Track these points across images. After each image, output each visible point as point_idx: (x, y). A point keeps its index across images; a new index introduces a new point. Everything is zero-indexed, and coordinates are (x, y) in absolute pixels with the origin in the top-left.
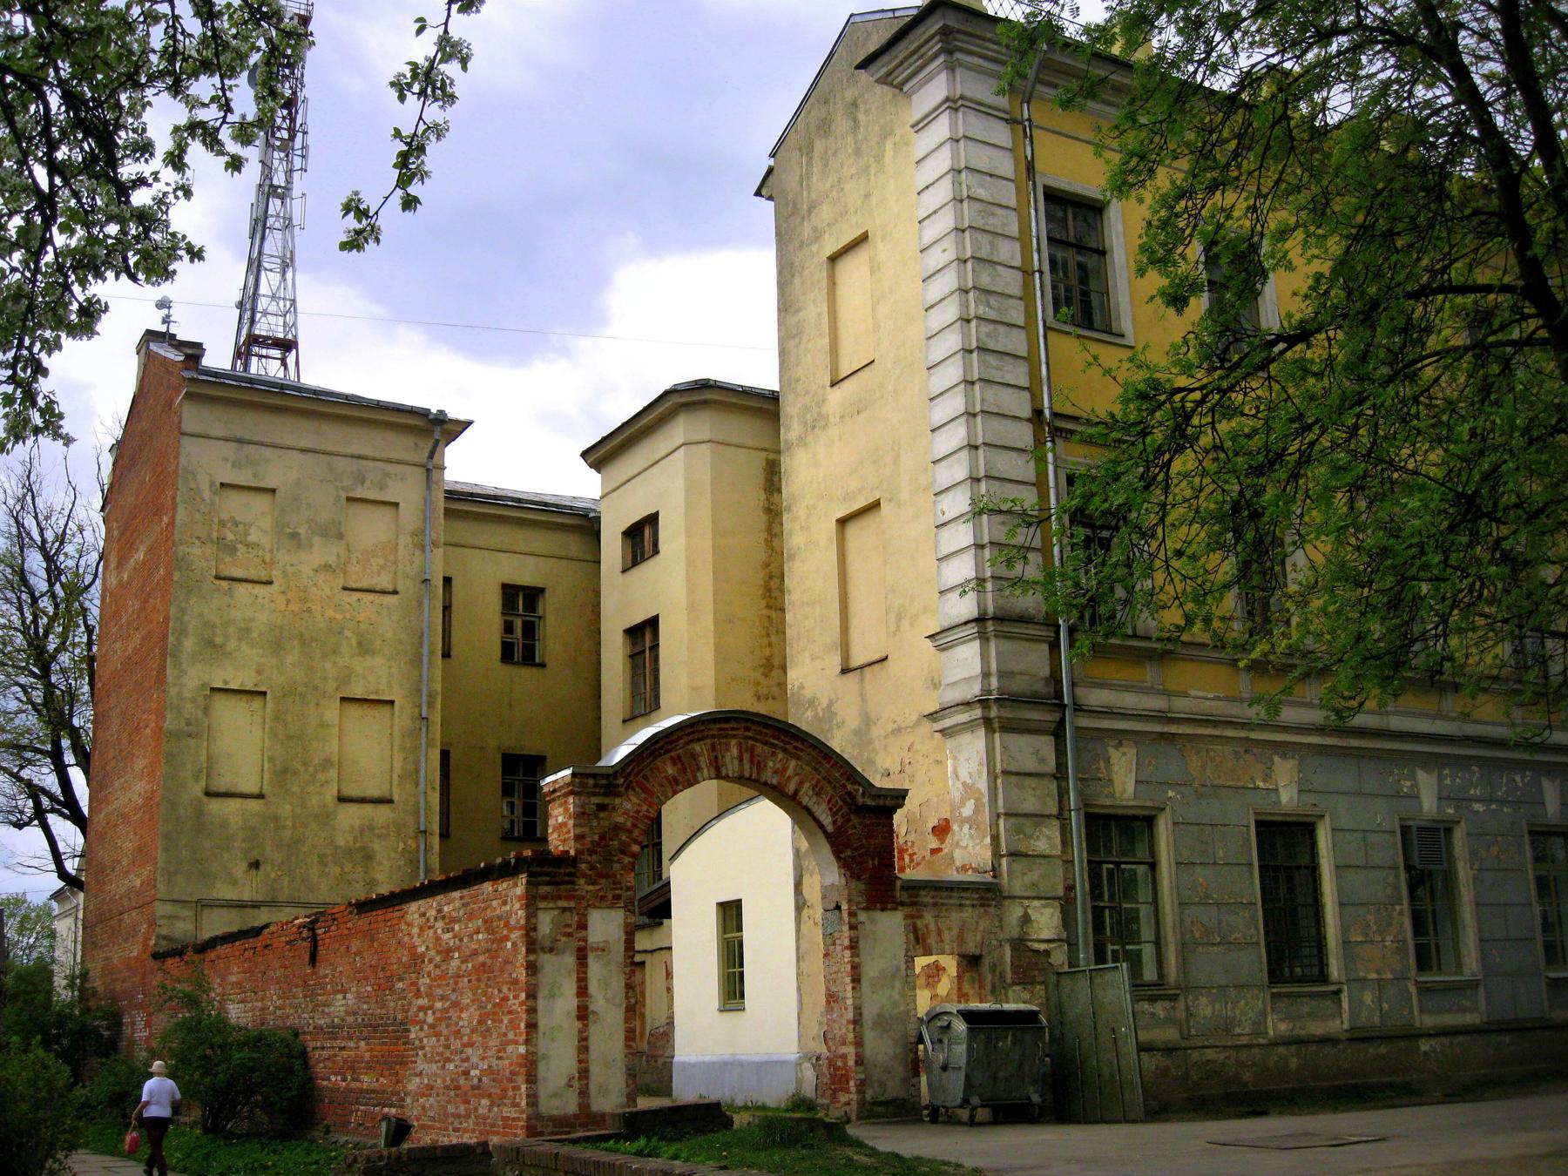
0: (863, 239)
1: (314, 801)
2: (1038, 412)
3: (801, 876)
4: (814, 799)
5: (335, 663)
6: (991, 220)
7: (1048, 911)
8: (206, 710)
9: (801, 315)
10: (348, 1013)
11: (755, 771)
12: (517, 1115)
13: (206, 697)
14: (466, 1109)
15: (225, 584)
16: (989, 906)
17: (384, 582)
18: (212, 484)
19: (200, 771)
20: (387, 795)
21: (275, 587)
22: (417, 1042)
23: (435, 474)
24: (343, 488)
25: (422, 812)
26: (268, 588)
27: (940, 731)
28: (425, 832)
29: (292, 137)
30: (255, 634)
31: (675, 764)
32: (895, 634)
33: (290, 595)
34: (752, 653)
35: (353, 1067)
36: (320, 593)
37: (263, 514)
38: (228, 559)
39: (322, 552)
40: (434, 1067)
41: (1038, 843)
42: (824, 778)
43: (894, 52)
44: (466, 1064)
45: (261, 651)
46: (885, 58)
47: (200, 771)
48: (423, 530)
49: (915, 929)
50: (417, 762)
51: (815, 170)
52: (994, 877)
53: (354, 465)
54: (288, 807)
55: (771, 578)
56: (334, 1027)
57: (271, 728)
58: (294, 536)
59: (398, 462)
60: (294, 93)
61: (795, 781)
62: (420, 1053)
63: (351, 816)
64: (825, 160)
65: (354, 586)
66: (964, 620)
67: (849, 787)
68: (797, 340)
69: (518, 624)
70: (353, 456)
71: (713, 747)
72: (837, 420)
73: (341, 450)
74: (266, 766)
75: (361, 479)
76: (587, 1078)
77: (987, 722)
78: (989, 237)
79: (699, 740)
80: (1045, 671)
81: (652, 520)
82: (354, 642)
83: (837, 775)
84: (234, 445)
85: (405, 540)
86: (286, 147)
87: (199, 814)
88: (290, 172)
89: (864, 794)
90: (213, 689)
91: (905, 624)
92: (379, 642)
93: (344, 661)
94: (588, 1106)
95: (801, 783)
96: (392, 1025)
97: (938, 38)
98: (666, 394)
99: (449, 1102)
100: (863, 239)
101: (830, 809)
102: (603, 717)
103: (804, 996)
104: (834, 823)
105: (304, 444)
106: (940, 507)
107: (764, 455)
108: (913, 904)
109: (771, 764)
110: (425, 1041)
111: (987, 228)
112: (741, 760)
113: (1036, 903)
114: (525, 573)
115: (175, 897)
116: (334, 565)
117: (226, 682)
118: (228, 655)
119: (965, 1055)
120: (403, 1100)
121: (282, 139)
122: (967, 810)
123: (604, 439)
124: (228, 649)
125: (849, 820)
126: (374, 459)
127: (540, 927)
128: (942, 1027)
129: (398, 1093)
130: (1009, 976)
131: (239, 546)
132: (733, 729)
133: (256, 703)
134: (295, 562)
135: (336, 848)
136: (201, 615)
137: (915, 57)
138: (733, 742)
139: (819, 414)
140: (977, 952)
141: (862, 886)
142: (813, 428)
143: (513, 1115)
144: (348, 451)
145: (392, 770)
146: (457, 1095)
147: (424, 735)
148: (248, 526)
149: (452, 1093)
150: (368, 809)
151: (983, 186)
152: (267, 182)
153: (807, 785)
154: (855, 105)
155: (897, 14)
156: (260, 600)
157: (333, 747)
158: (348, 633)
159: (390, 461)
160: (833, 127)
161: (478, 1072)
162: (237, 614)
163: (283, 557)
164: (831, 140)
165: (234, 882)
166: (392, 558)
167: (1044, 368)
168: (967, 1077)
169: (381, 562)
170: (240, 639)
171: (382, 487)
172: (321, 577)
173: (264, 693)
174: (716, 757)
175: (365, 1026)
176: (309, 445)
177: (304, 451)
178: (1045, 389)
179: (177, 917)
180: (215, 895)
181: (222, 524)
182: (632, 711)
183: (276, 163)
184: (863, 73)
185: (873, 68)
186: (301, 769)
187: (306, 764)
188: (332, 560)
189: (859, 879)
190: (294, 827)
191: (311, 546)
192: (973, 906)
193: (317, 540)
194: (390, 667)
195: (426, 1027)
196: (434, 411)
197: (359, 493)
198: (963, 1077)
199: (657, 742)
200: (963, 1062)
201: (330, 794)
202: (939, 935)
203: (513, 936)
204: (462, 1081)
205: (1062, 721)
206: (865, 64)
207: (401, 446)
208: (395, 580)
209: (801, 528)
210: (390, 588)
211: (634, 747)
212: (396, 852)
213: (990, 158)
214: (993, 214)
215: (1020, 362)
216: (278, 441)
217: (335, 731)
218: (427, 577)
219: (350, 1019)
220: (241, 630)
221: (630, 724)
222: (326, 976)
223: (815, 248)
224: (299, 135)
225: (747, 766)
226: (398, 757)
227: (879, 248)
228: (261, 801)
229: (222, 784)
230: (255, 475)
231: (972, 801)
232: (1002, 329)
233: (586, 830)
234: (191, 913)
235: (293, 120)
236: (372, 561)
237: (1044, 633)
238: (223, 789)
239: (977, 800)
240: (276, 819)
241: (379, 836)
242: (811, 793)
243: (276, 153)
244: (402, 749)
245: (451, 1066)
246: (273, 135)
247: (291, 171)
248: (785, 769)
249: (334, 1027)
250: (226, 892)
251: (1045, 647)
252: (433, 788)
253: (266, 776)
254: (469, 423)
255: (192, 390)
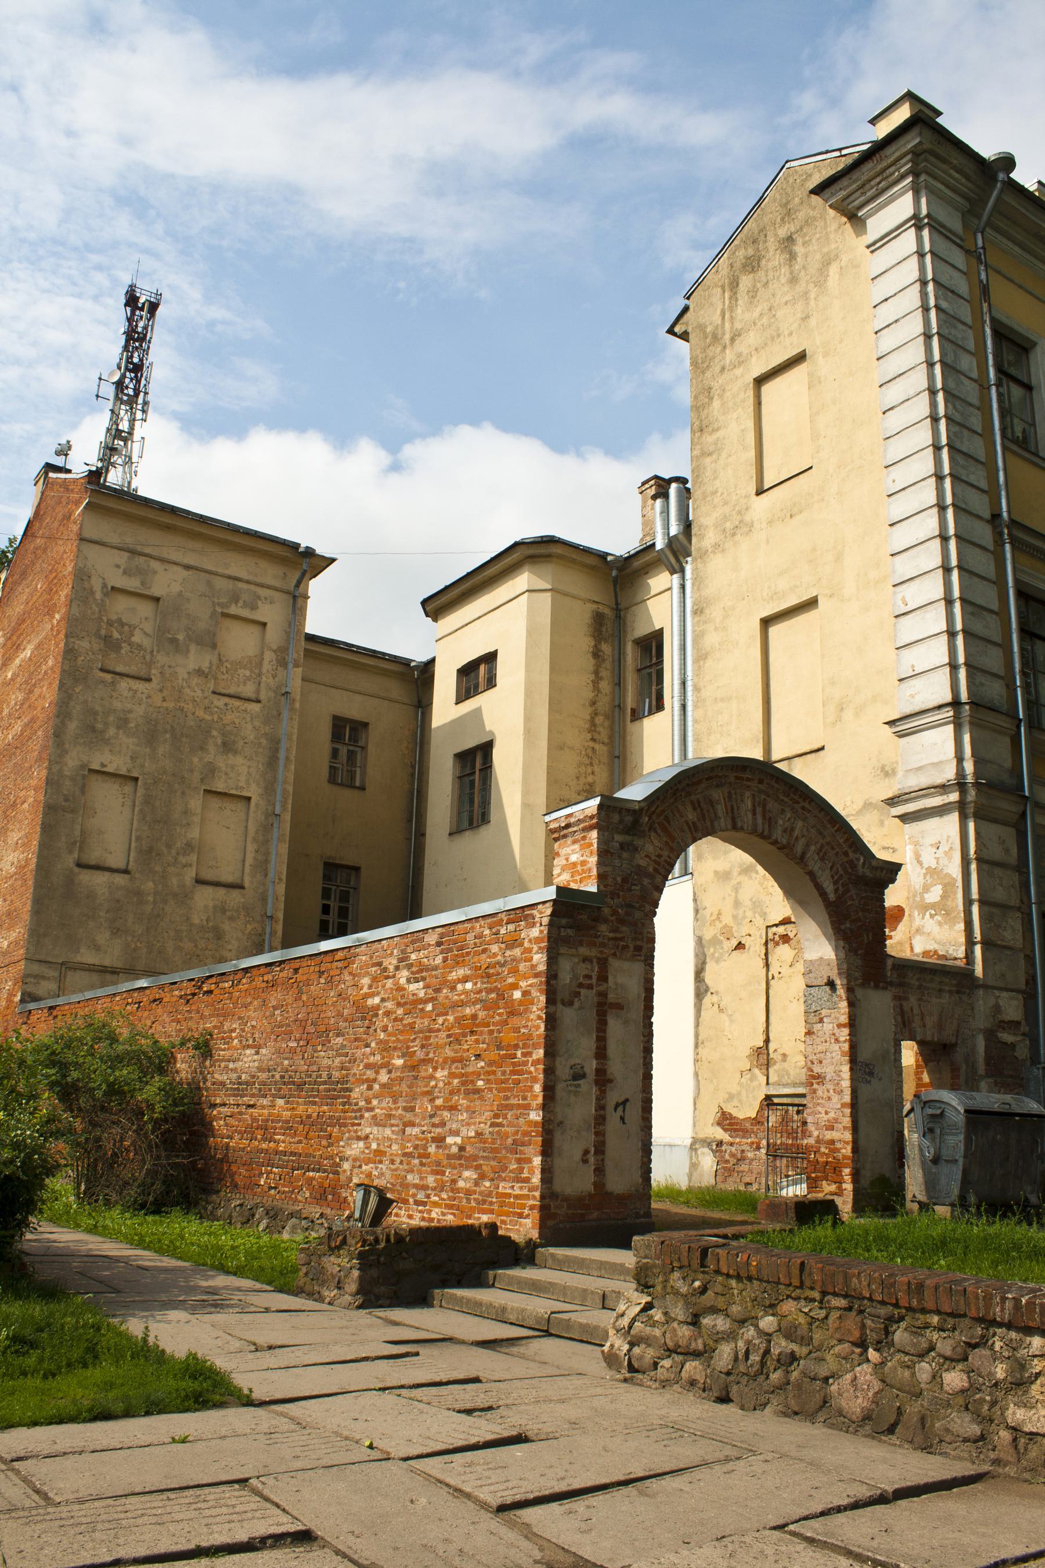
0: (800, 358)
1: (175, 881)
2: (996, 516)
3: (704, 963)
4: (819, 864)
5: (201, 759)
6: (953, 332)
7: (1015, 1003)
8: (83, 791)
9: (720, 434)
10: (260, 1069)
11: (766, 827)
12: (525, 1192)
13: (84, 777)
14: (436, 1180)
15: (108, 677)
16: (964, 993)
17: (248, 690)
18: (105, 586)
19: (74, 843)
20: (239, 881)
21: (154, 684)
22: (362, 1103)
23: (300, 601)
24: (219, 604)
25: (270, 900)
26: (147, 685)
27: (898, 817)
28: (271, 917)
29: (137, 395)
30: (132, 725)
31: (695, 809)
32: (834, 724)
33: (166, 693)
34: (578, 778)
35: (265, 1129)
36: (192, 694)
37: (146, 619)
38: (113, 655)
39: (197, 659)
40: (388, 1132)
41: (1005, 934)
42: (828, 843)
43: (855, 175)
44: (439, 1130)
45: (136, 740)
46: (845, 182)
47: (74, 843)
48: (287, 649)
49: (902, 1013)
50: (267, 854)
51: (740, 302)
52: (968, 964)
53: (228, 585)
54: (151, 884)
55: (596, 714)
56: (240, 1084)
57: (141, 811)
58: (174, 641)
59: (269, 587)
60: (141, 360)
61: (802, 842)
62: (367, 1115)
63: (205, 898)
64: (753, 293)
65: (223, 691)
66: (936, 703)
67: (852, 855)
68: (714, 457)
69: (343, 751)
70: (230, 577)
71: (730, 796)
72: (764, 525)
73: (220, 570)
74: (133, 845)
75: (235, 598)
76: (603, 1152)
77: (961, 806)
78: (954, 347)
79: (717, 786)
80: (1008, 764)
81: (490, 658)
82: (219, 741)
83: (841, 841)
84: (127, 554)
85: (269, 656)
86: (132, 401)
87: (70, 881)
88: (132, 421)
89: (864, 863)
90: (90, 770)
91: (848, 715)
92: (241, 743)
93: (209, 758)
94: (604, 1185)
95: (808, 845)
96: (325, 1083)
97: (909, 157)
98: (516, 545)
99: (411, 1171)
100: (800, 358)
101: (833, 877)
102: (429, 831)
103: (702, 1082)
104: (836, 890)
105: (190, 559)
106: (899, 596)
107: (595, 606)
108: (901, 985)
109: (781, 822)
110: (375, 1102)
111: (950, 337)
112: (754, 814)
113: (1005, 994)
114: (354, 708)
115: (42, 957)
116: (206, 671)
117: (103, 765)
118: (107, 742)
119: (962, 1146)
120: (338, 1165)
121: (128, 395)
122: (934, 895)
123: (447, 588)
124: (107, 736)
125: (848, 891)
126: (248, 582)
127: (561, 975)
128: (933, 1116)
129: (331, 1157)
130: (981, 1068)
131: (124, 645)
132: (748, 780)
133: (128, 788)
134: (174, 664)
135: (192, 925)
136: (85, 702)
137: (878, 179)
138: (747, 794)
139: (741, 522)
140: (953, 1040)
141: (859, 962)
142: (734, 535)
143: (517, 1192)
144: (227, 572)
145: (244, 861)
146: (422, 1164)
147: (275, 830)
148: (132, 628)
149: (416, 1161)
150: (222, 891)
151: (946, 300)
152: (114, 427)
153: (813, 848)
154: (790, 239)
155: (844, 152)
156: (139, 694)
157: (194, 833)
158: (215, 733)
159: (261, 585)
160: (763, 262)
161: (459, 1140)
162: (117, 705)
163: (162, 659)
164: (761, 274)
165: (97, 948)
166: (257, 671)
167: (1001, 474)
168: (965, 1172)
169: (248, 673)
170: (118, 728)
171: (254, 608)
172: (195, 681)
173: (136, 779)
174: (732, 808)
175: (284, 1083)
176: (192, 563)
177: (187, 567)
178: (1003, 493)
179: (44, 978)
180: (79, 958)
181: (110, 623)
182: (458, 827)
183: (122, 413)
184: (814, 198)
185: (827, 192)
186: (165, 851)
187: (169, 846)
188: (205, 665)
189: (856, 954)
190: (155, 902)
191: (188, 651)
192: (950, 992)
193: (193, 648)
194: (249, 767)
195: (376, 1087)
196: (303, 545)
197: (233, 610)
198: (960, 1173)
199: (680, 782)
200: (959, 1156)
201: (190, 874)
202: (922, 1019)
203: (523, 984)
204: (432, 1149)
205: (1023, 815)
206: (818, 190)
207: (270, 573)
208: (258, 692)
209: (716, 629)
210: (253, 696)
211: (662, 783)
212: (243, 933)
213: (951, 278)
214: (955, 327)
215: (980, 466)
216: (165, 555)
217: (197, 819)
218: (288, 690)
219: (263, 1076)
220: (120, 719)
221: (456, 837)
222: (234, 1030)
223: (738, 372)
224: (142, 394)
225: (760, 821)
226: (251, 848)
227: (818, 365)
228: (127, 876)
229: (93, 857)
230: (143, 583)
231: (940, 887)
232: (966, 432)
233: (609, 869)
234: (56, 974)
235: (139, 382)
236: (240, 671)
237: (1005, 725)
238: (93, 863)
239: (946, 887)
240: (139, 893)
241: (231, 918)
242: (816, 857)
243: (123, 407)
244: (255, 840)
245: (415, 1131)
246: (122, 392)
247: (134, 420)
248: (793, 829)
249: (240, 1084)
250: (88, 957)
251: (1008, 740)
252: (280, 879)
253: (132, 854)
254: (333, 560)
255: (93, 500)
